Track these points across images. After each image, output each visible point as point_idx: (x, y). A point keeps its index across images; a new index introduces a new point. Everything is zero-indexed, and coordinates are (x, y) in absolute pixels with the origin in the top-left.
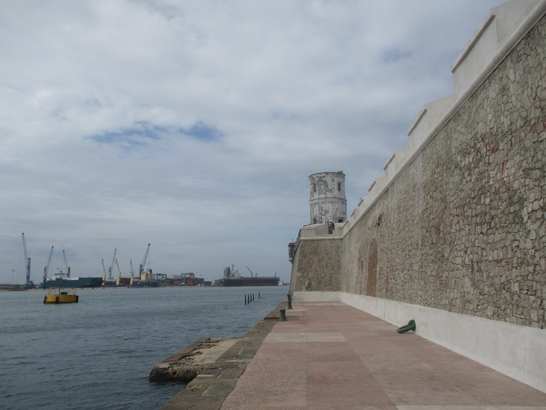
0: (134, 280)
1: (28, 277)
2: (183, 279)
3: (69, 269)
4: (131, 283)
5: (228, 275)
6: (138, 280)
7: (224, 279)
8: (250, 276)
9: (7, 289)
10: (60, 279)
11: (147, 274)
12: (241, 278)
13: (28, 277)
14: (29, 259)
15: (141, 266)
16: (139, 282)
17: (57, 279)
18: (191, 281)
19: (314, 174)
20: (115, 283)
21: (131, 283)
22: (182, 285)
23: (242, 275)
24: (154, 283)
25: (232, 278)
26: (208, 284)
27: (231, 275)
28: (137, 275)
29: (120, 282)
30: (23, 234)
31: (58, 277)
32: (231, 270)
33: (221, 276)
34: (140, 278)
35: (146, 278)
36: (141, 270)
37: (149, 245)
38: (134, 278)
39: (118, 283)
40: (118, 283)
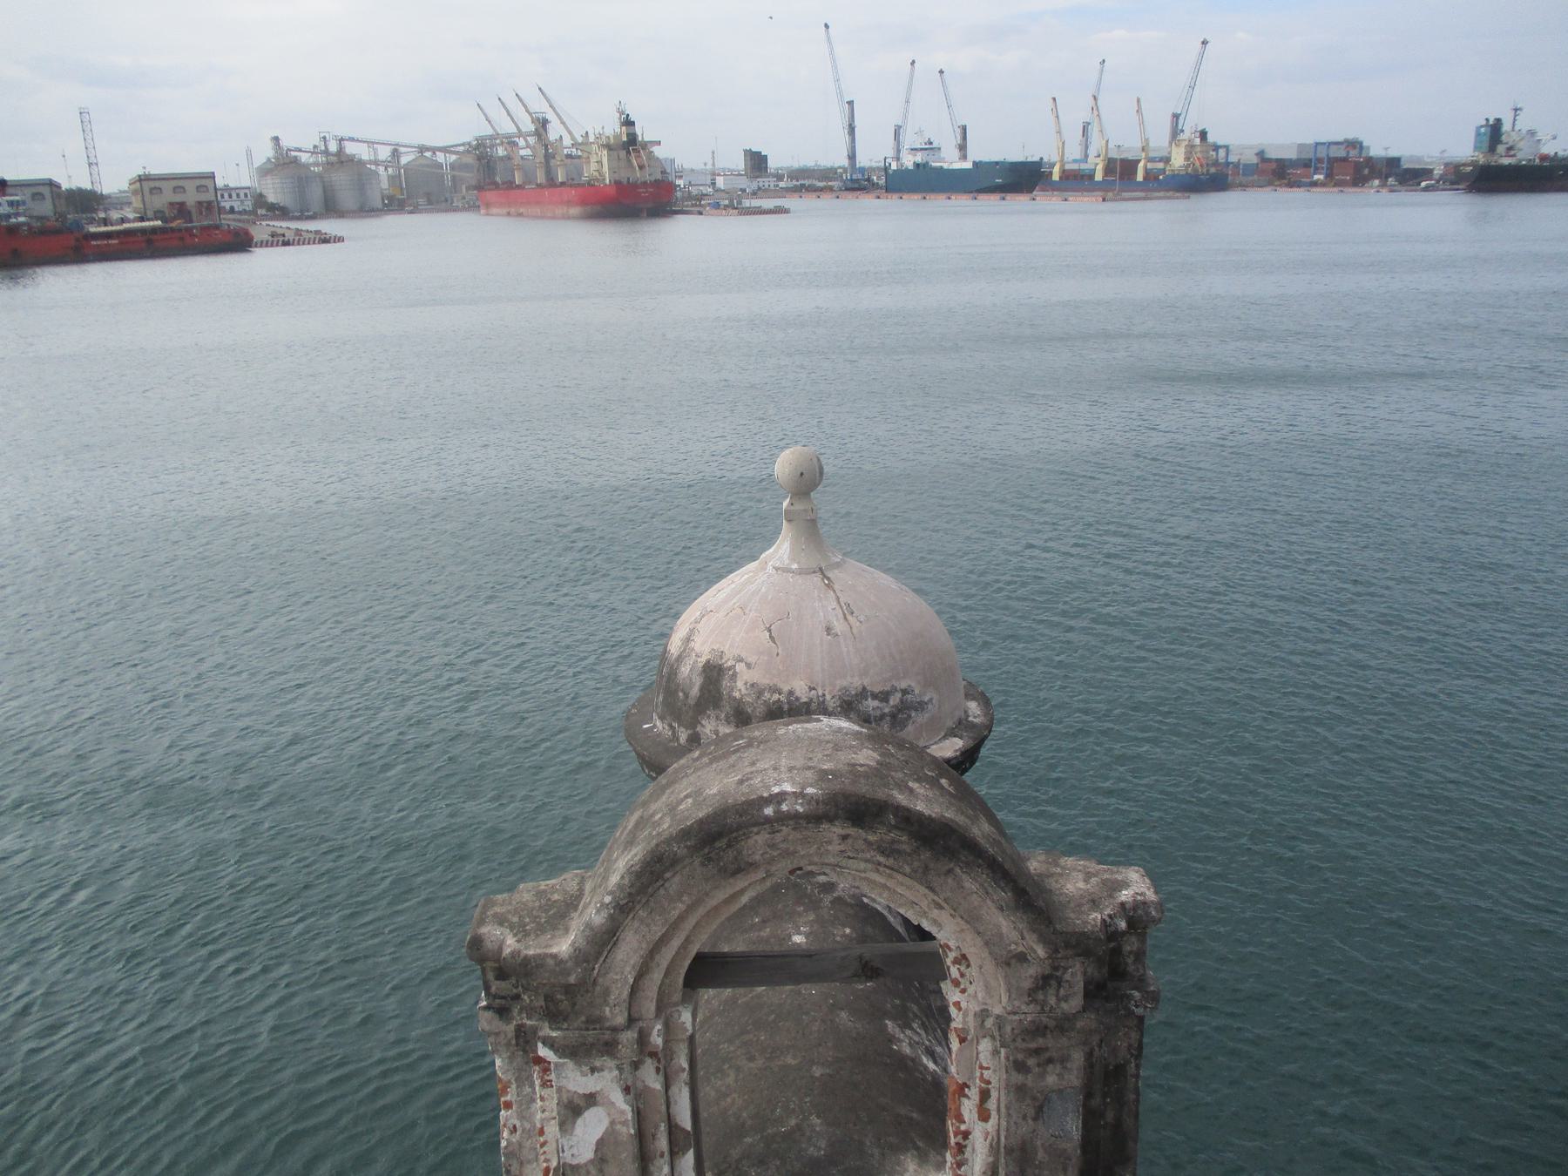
0: (1150, 166)
1: (852, 157)
2: (1320, 160)
3: (964, 129)
4: (1140, 178)
5: (1492, 149)
6: (1161, 165)
7: (1473, 163)
8: (89, 187)
9: (811, 189)
10: (925, 165)
11: (1191, 147)
12: (1544, 158)
13: (852, 157)
14: (851, 103)
15: (1176, 117)
16: (1163, 171)
17: (917, 165)
18: (1351, 168)
19: (352, 139)
20: (1091, 176)
21: (1140, 178)
22: (1315, 184)
23: (1549, 149)
24: (1210, 176)
25: (1506, 161)
26: (1401, 175)
27: (1501, 149)
28: (1073, 152)
29: (1109, 170)
30: (826, 26)
31: (919, 158)
32: (1506, 127)
33: (1464, 149)
34: (1167, 160)
35: (1187, 159)
36: (1175, 132)
37: (1204, 43)
38: (1152, 160)
39: (1099, 177)
40: (1099, 177)
